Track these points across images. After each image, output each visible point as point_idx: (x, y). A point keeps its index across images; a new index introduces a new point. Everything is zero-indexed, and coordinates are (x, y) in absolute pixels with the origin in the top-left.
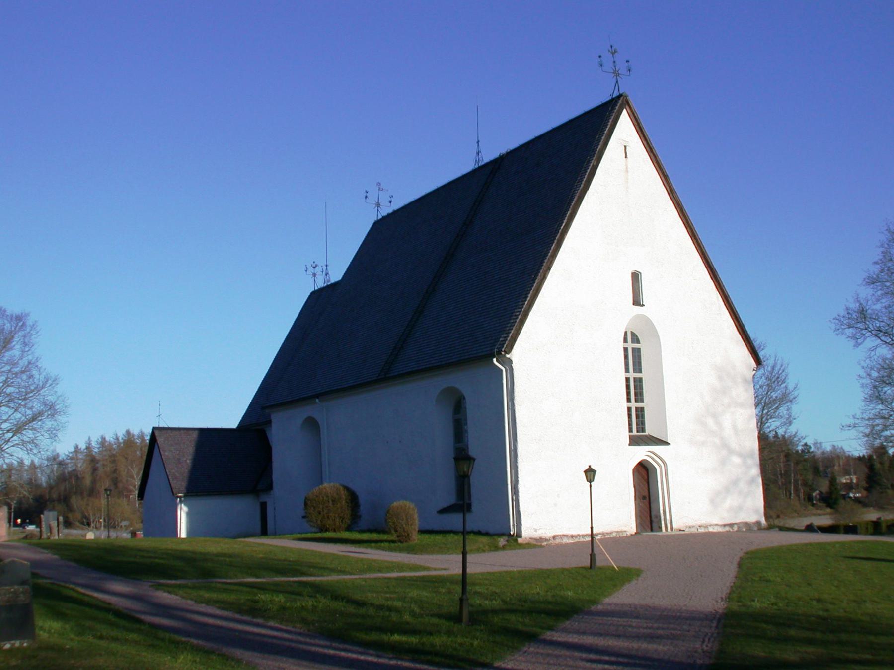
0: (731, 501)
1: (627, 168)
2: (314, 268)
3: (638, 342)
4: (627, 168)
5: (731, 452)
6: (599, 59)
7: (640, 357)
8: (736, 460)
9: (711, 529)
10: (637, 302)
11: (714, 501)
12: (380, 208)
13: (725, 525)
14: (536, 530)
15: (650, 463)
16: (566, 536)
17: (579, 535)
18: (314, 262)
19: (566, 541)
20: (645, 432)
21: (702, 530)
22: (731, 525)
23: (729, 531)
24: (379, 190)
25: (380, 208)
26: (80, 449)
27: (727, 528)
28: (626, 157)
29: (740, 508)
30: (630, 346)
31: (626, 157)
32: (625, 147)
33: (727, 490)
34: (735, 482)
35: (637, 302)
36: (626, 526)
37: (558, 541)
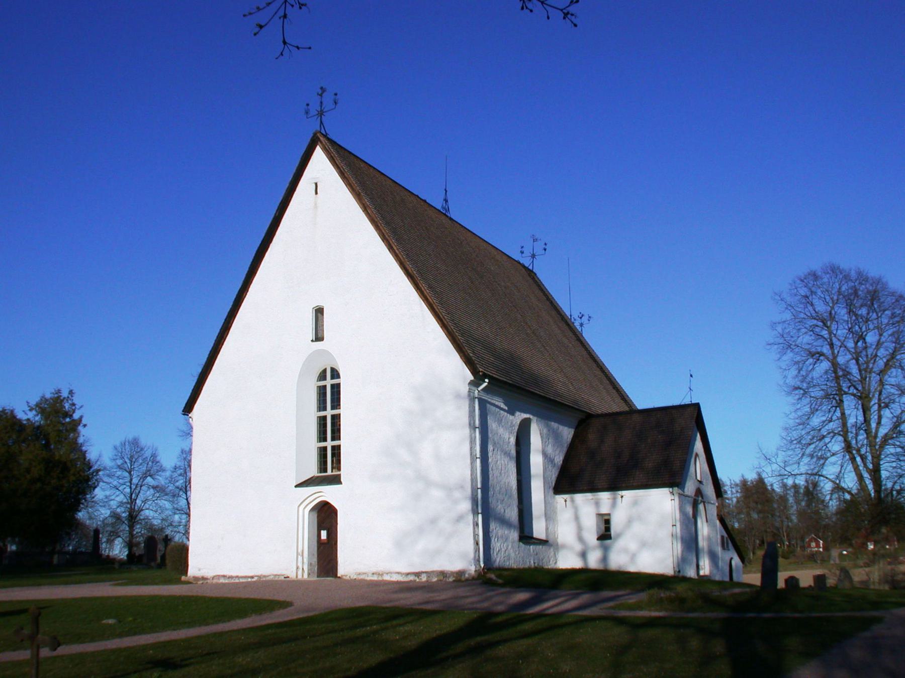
0: (424, 543)
1: (316, 204)
2: (581, 318)
3: (338, 376)
4: (316, 204)
5: (429, 483)
6: (306, 107)
7: (339, 393)
8: (437, 493)
9: (387, 578)
10: (319, 338)
11: (400, 544)
12: (536, 258)
13: (408, 574)
14: (199, 570)
15: (316, 504)
16: (224, 576)
17: (237, 577)
18: (580, 313)
19: (222, 581)
20: (326, 472)
21: (375, 578)
22: (418, 574)
23: (415, 581)
24: (534, 241)
25: (536, 258)
26: (77, 514)
27: (411, 578)
28: (316, 193)
29: (437, 552)
30: (329, 382)
31: (316, 193)
32: (316, 184)
33: (421, 530)
34: (433, 521)
35: (319, 338)
36: (286, 570)
37: (215, 581)
